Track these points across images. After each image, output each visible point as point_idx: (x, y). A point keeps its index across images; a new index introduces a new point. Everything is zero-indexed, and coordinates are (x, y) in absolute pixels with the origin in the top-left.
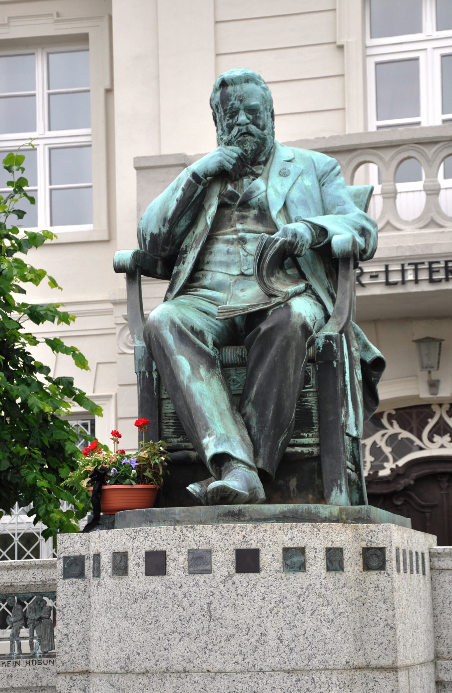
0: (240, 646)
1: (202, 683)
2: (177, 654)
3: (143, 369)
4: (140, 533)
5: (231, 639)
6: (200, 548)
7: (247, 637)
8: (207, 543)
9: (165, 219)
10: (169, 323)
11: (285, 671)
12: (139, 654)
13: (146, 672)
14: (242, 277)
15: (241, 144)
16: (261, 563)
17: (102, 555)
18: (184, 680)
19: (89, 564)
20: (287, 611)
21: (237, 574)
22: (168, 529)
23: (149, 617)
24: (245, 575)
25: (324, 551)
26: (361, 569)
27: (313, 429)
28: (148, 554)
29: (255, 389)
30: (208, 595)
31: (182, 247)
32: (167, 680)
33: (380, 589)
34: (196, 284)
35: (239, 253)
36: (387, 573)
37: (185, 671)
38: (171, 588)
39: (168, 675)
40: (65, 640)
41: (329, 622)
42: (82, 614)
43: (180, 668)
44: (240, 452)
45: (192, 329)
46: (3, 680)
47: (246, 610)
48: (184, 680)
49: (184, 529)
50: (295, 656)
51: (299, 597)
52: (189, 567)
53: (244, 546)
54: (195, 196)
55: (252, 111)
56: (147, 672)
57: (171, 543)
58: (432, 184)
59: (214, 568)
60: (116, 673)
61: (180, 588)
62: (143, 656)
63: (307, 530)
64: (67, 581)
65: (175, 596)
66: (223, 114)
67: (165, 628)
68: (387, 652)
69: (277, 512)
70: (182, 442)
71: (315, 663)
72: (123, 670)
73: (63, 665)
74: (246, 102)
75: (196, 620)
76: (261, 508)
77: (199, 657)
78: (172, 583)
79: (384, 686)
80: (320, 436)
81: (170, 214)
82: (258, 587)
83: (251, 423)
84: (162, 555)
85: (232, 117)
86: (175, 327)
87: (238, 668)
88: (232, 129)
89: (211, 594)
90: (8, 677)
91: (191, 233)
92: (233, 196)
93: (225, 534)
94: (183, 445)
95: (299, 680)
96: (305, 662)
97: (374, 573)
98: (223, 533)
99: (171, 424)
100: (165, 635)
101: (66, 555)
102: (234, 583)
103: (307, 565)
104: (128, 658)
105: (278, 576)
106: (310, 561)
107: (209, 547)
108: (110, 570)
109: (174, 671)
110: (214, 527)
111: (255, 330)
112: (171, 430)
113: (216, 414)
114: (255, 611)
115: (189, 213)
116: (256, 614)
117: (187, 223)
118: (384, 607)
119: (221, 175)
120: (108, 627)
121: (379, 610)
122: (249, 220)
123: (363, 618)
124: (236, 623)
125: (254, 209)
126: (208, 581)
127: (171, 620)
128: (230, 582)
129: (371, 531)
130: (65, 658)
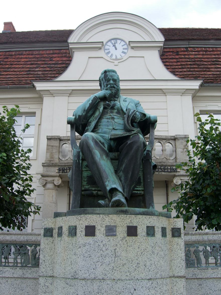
0: (128, 268)
1: (111, 284)
2: (99, 272)
3: (76, 159)
4: (83, 217)
5: (124, 265)
6: (111, 225)
7: (132, 264)
8: (114, 223)
9: (84, 110)
10: (92, 138)
11: (147, 279)
12: (81, 271)
13: (84, 279)
14: (114, 130)
15: (110, 90)
16: (138, 232)
17: (63, 227)
18: (103, 283)
19: (55, 232)
20: (148, 253)
21: (128, 237)
22: (96, 216)
23: (86, 255)
24: (131, 237)
25: (161, 228)
26: (171, 236)
27: (141, 185)
28: (87, 227)
29: (124, 166)
30: (114, 246)
31: (89, 121)
32: (94, 283)
33: (179, 245)
34: (120, 108)
35: (112, 122)
36: (182, 238)
37: (103, 279)
38: (97, 242)
39: (95, 280)
40: (44, 263)
41: (162, 258)
42: (51, 252)
43: (101, 278)
44: (120, 189)
45: (100, 141)
46: (11, 274)
47: (131, 253)
48: (103, 283)
49: (104, 216)
50: (151, 273)
51: (152, 247)
52: (106, 233)
53: (131, 225)
54: (96, 103)
55: (115, 80)
56: (85, 279)
57: (98, 222)
58: (74, 182)
59: (118, 234)
60: (69, 278)
61: (101, 242)
62: (83, 272)
63: (155, 219)
64: (45, 238)
65: (99, 246)
66: (104, 81)
67: (94, 260)
68: (182, 270)
69: (141, 212)
70: (89, 187)
71: (158, 276)
72: (72, 277)
73: (42, 273)
74: (113, 78)
75: (109, 256)
76: (134, 209)
77: (110, 273)
78: (98, 240)
79: (180, 284)
80: (144, 187)
81: (86, 108)
82: (136, 242)
83: (121, 179)
84: (94, 227)
85: (108, 82)
86: (94, 140)
87: (127, 278)
88: (108, 85)
89: (116, 245)
90: (13, 273)
91: (93, 117)
92: (109, 105)
93: (123, 219)
94: (90, 188)
95: (152, 283)
96: (155, 276)
97: (177, 238)
98: (122, 219)
99: (86, 180)
100: (94, 263)
101: (45, 227)
102: (126, 241)
103: (155, 234)
104: (76, 272)
105: (144, 238)
106: (156, 232)
107: (115, 224)
108: (67, 234)
109: (98, 279)
110: (118, 216)
111: (125, 143)
112: (86, 183)
113: (110, 173)
114: (135, 253)
115: (93, 109)
116: (136, 254)
117: (92, 113)
118: (181, 252)
119: (104, 99)
120: (65, 258)
121: (178, 253)
122: (114, 113)
123: (172, 257)
124: (127, 258)
125: (116, 110)
126: (114, 239)
127: (97, 256)
128: (125, 240)
129: (175, 221)
130: (43, 270)
